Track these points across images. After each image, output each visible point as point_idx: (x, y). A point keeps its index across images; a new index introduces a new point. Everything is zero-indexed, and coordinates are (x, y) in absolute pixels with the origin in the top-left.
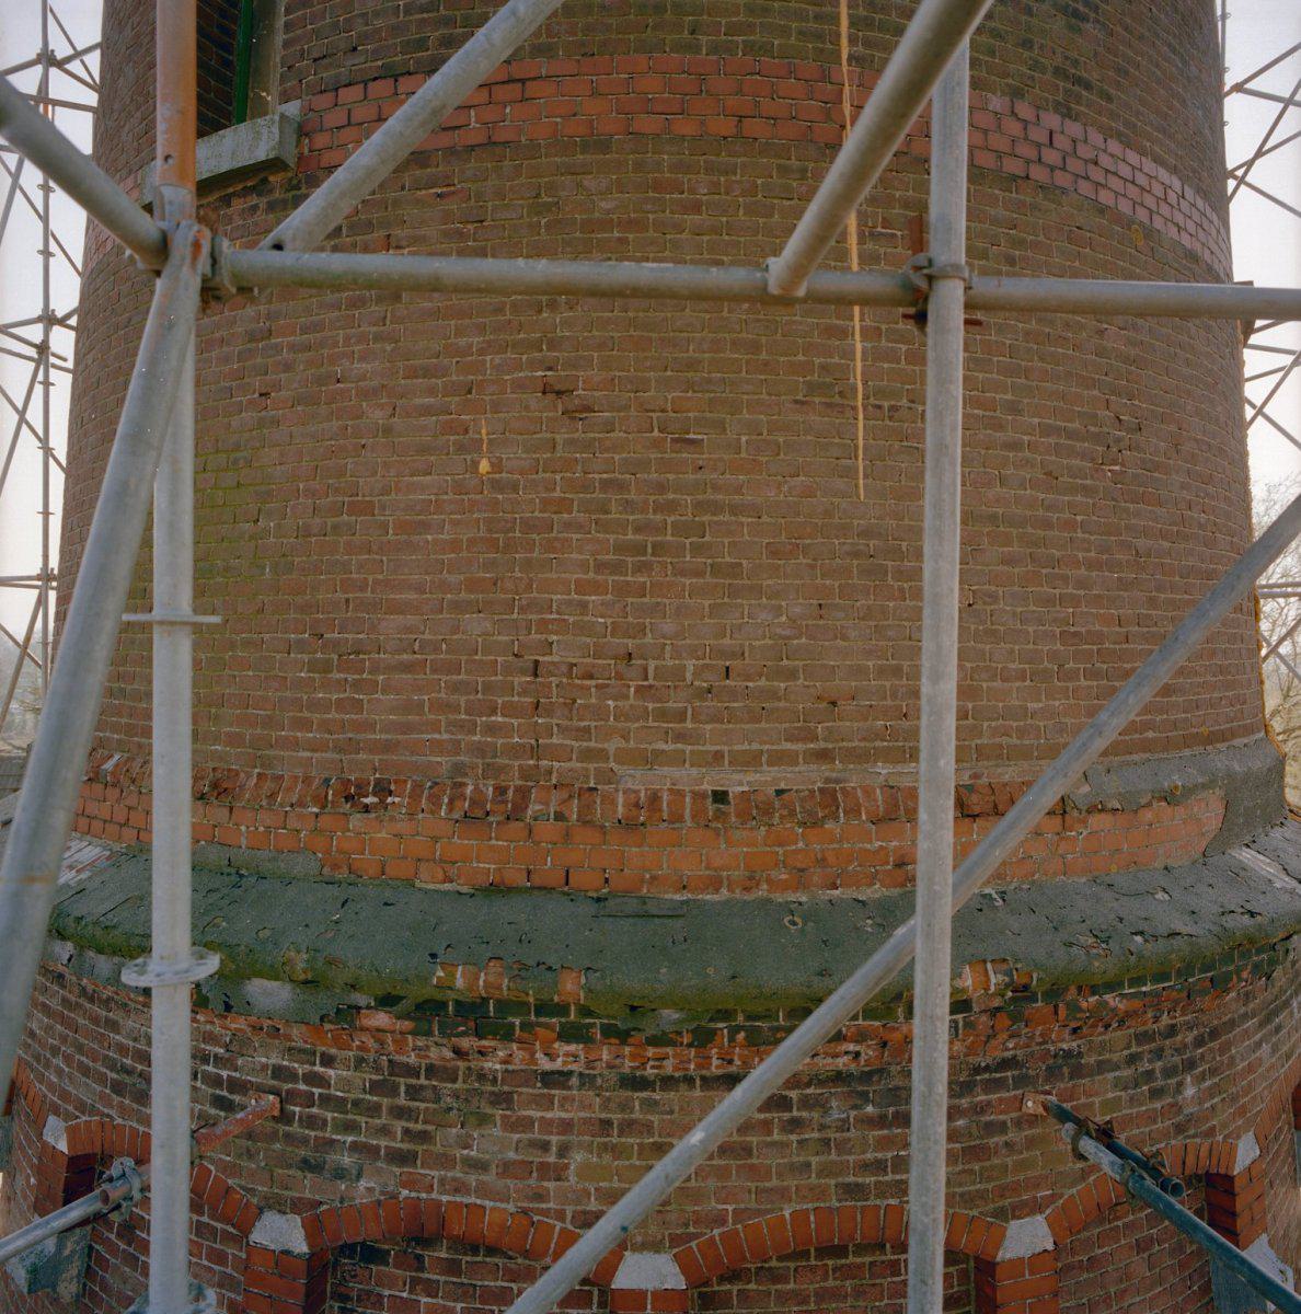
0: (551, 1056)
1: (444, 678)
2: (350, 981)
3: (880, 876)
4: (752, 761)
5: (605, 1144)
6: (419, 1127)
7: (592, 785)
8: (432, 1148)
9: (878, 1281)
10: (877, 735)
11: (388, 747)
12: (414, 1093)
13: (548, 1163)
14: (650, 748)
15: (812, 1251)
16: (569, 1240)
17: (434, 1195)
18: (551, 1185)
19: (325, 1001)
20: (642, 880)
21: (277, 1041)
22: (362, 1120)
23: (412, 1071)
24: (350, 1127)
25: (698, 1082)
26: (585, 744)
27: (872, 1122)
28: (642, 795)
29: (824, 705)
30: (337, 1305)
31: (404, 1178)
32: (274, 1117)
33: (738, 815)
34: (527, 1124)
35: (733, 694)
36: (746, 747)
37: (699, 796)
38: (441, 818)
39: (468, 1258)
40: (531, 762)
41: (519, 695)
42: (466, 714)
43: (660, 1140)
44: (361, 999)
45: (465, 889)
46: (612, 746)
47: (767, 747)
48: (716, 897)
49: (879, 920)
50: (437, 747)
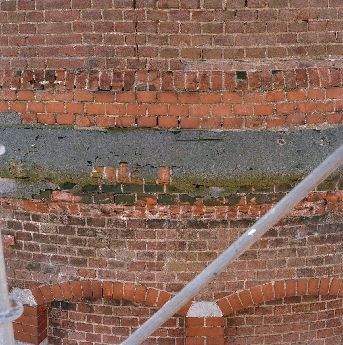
0: (153, 213)
1: (81, 10)
2: (47, 176)
3: (328, 117)
4: (259, 54)
5: (182, 254)
6: (87, 248)
7: (169, 70)
8: (94, 257)
9: (314, 312)
10: (330, 39)
11: (52, 52)
12: (82, 232)
13: (153, 263)
14: (202, 48)
15: (283, 299)
16: (164, 299)
17: (97, 279)
18: (155, 273)
19: (34, 188)
20: (199, 122)
21: (9, 210)
22: (57, 246)
23: (81, 222)
24: (51, 249)
25: (229, 223)
26: (165, 46)
27: (317, 241)
28: (198, 75)
29: (300, 22)
30: (52, 327)
31: (81, 271)
32: (11, 246)
33: (252, 85)
34: (142, 245)
35: (249, 15)
36: (256, 46)
37: (230, 75)
38: (86, 91)
39: (115, 307)
40: (134, 58)
41: (125, 19)
42: (95, 31)
43: (210, 251)
44: (52, 186)
45: (101, 129)
46: (181, 47)
47: (267, 46)
48: (239, 130)
49: (327, 140)
50: (80, 51)
